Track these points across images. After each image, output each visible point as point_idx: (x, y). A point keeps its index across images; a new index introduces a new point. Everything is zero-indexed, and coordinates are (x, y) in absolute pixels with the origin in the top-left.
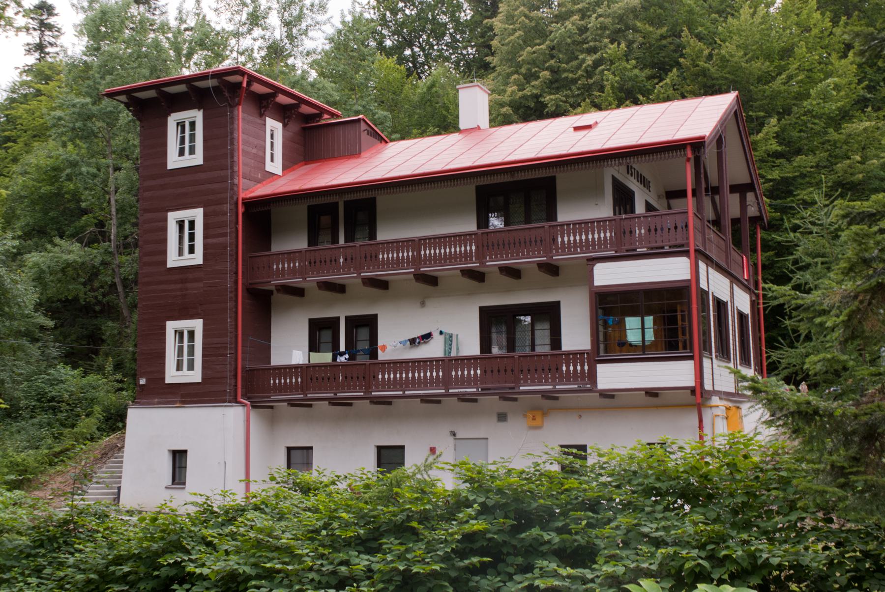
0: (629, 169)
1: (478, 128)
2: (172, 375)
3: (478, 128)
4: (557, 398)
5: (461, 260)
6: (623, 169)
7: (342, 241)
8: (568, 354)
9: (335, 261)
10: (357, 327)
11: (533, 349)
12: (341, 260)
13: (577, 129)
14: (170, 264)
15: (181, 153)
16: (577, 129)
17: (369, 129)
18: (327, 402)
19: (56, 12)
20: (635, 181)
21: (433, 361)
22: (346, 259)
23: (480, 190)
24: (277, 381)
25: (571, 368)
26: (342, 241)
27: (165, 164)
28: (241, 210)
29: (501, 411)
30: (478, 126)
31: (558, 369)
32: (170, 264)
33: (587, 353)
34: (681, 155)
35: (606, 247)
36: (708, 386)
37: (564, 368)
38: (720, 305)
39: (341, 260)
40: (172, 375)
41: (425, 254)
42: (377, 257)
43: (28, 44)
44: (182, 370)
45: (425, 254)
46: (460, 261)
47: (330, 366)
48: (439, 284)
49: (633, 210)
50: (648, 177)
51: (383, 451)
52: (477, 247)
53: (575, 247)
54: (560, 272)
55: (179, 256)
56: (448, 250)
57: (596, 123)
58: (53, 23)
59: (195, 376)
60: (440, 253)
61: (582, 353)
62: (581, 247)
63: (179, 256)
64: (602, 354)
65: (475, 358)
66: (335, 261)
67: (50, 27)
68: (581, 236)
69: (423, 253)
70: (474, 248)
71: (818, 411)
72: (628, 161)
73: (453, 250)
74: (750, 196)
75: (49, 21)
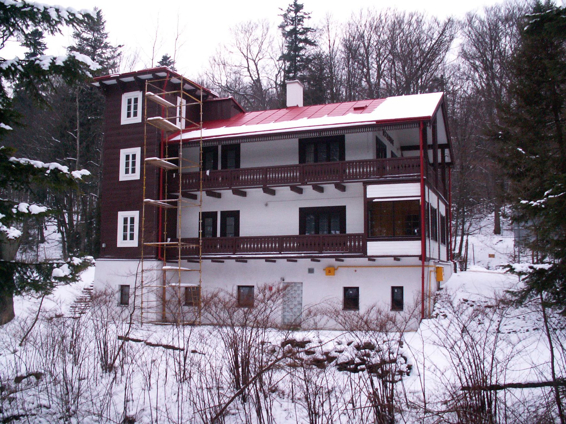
0: (384, 133)
1: (297, 106)
2: (121, 243)
3: (297, 106)
4: (374, 260)
5: (281, 182)
6: (381, 132)
7: (220, 168)
8: (351, 235)
9: (217, 179)
10: (208, 217)
11: (330, 232)
12: (220, 179)
13: (356, 109)
14: (121, 179)
15: (129, 115)
16: (356, 109)
17: (235, 105)
18: (310, 259)
19: (43, 36)
20: (387, 140)
21: (360, 236)
22: (222, 179)
23: (301, 142)
24: (353, 244)
25: (357, 244)
26: (220, 168)
27: (120, 122)
28: (167, 147)
29: (310, 267)
30: (297, 105)
31: (345, 244)
32: (121, 179)
33: (362, 236)
34: (408, 127)
35: (296, 180)
36: (428, 256)
37: (348, 244)
38: (434, 211)
39: (220, 179)
40: (121, 243)
41: (270, 177)
42: (238, 178)
43: (27, 53)
44: (126, 240)
45: (270, 177)
46: (278, 182)
47: (339, 236)
48: (303, 192)
49: (385, 156)
50: (393, 137)
51: (356, 290)
52: (300, 173)
53: (360, 175)
54: (346, 189)
55: (126, 173)
56: (355, 170)
57: (366, 106)
58: (41, 41)
59: (134, 243)
60: (356, 171)
61: (359, 235)
62: (360, 175)
63: (126, 173)
64: (370, 236)
65: (296, 236)
66: (217, 179)
67: (40, 44)
68: (272, 176)
69: (268, 176)
70: (298, 174)
71: (511, 272)
72: (383, 128)
73: (368, 170)
74: (447, 151)
75: (39, 40)
